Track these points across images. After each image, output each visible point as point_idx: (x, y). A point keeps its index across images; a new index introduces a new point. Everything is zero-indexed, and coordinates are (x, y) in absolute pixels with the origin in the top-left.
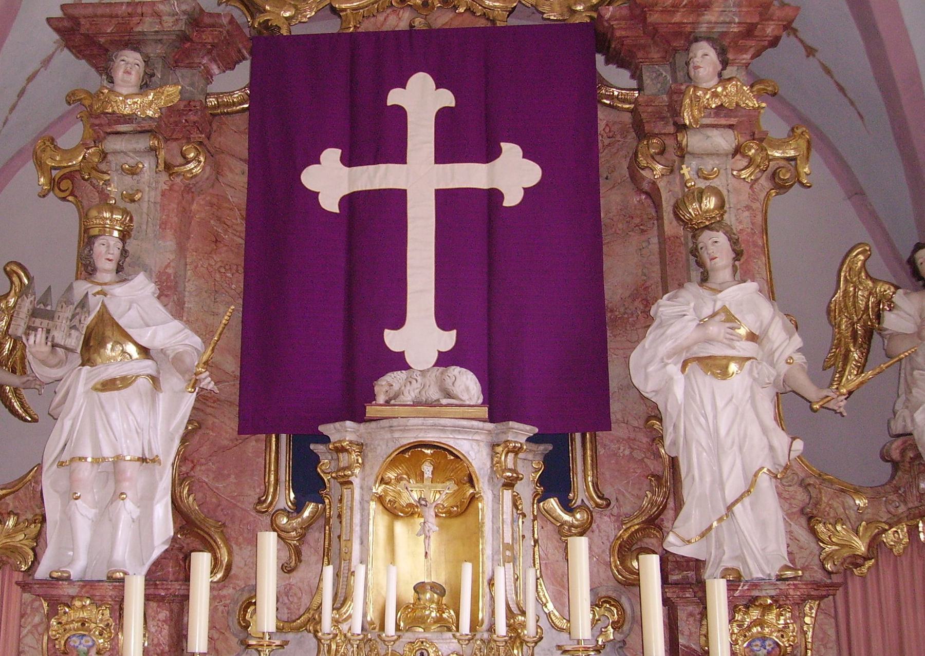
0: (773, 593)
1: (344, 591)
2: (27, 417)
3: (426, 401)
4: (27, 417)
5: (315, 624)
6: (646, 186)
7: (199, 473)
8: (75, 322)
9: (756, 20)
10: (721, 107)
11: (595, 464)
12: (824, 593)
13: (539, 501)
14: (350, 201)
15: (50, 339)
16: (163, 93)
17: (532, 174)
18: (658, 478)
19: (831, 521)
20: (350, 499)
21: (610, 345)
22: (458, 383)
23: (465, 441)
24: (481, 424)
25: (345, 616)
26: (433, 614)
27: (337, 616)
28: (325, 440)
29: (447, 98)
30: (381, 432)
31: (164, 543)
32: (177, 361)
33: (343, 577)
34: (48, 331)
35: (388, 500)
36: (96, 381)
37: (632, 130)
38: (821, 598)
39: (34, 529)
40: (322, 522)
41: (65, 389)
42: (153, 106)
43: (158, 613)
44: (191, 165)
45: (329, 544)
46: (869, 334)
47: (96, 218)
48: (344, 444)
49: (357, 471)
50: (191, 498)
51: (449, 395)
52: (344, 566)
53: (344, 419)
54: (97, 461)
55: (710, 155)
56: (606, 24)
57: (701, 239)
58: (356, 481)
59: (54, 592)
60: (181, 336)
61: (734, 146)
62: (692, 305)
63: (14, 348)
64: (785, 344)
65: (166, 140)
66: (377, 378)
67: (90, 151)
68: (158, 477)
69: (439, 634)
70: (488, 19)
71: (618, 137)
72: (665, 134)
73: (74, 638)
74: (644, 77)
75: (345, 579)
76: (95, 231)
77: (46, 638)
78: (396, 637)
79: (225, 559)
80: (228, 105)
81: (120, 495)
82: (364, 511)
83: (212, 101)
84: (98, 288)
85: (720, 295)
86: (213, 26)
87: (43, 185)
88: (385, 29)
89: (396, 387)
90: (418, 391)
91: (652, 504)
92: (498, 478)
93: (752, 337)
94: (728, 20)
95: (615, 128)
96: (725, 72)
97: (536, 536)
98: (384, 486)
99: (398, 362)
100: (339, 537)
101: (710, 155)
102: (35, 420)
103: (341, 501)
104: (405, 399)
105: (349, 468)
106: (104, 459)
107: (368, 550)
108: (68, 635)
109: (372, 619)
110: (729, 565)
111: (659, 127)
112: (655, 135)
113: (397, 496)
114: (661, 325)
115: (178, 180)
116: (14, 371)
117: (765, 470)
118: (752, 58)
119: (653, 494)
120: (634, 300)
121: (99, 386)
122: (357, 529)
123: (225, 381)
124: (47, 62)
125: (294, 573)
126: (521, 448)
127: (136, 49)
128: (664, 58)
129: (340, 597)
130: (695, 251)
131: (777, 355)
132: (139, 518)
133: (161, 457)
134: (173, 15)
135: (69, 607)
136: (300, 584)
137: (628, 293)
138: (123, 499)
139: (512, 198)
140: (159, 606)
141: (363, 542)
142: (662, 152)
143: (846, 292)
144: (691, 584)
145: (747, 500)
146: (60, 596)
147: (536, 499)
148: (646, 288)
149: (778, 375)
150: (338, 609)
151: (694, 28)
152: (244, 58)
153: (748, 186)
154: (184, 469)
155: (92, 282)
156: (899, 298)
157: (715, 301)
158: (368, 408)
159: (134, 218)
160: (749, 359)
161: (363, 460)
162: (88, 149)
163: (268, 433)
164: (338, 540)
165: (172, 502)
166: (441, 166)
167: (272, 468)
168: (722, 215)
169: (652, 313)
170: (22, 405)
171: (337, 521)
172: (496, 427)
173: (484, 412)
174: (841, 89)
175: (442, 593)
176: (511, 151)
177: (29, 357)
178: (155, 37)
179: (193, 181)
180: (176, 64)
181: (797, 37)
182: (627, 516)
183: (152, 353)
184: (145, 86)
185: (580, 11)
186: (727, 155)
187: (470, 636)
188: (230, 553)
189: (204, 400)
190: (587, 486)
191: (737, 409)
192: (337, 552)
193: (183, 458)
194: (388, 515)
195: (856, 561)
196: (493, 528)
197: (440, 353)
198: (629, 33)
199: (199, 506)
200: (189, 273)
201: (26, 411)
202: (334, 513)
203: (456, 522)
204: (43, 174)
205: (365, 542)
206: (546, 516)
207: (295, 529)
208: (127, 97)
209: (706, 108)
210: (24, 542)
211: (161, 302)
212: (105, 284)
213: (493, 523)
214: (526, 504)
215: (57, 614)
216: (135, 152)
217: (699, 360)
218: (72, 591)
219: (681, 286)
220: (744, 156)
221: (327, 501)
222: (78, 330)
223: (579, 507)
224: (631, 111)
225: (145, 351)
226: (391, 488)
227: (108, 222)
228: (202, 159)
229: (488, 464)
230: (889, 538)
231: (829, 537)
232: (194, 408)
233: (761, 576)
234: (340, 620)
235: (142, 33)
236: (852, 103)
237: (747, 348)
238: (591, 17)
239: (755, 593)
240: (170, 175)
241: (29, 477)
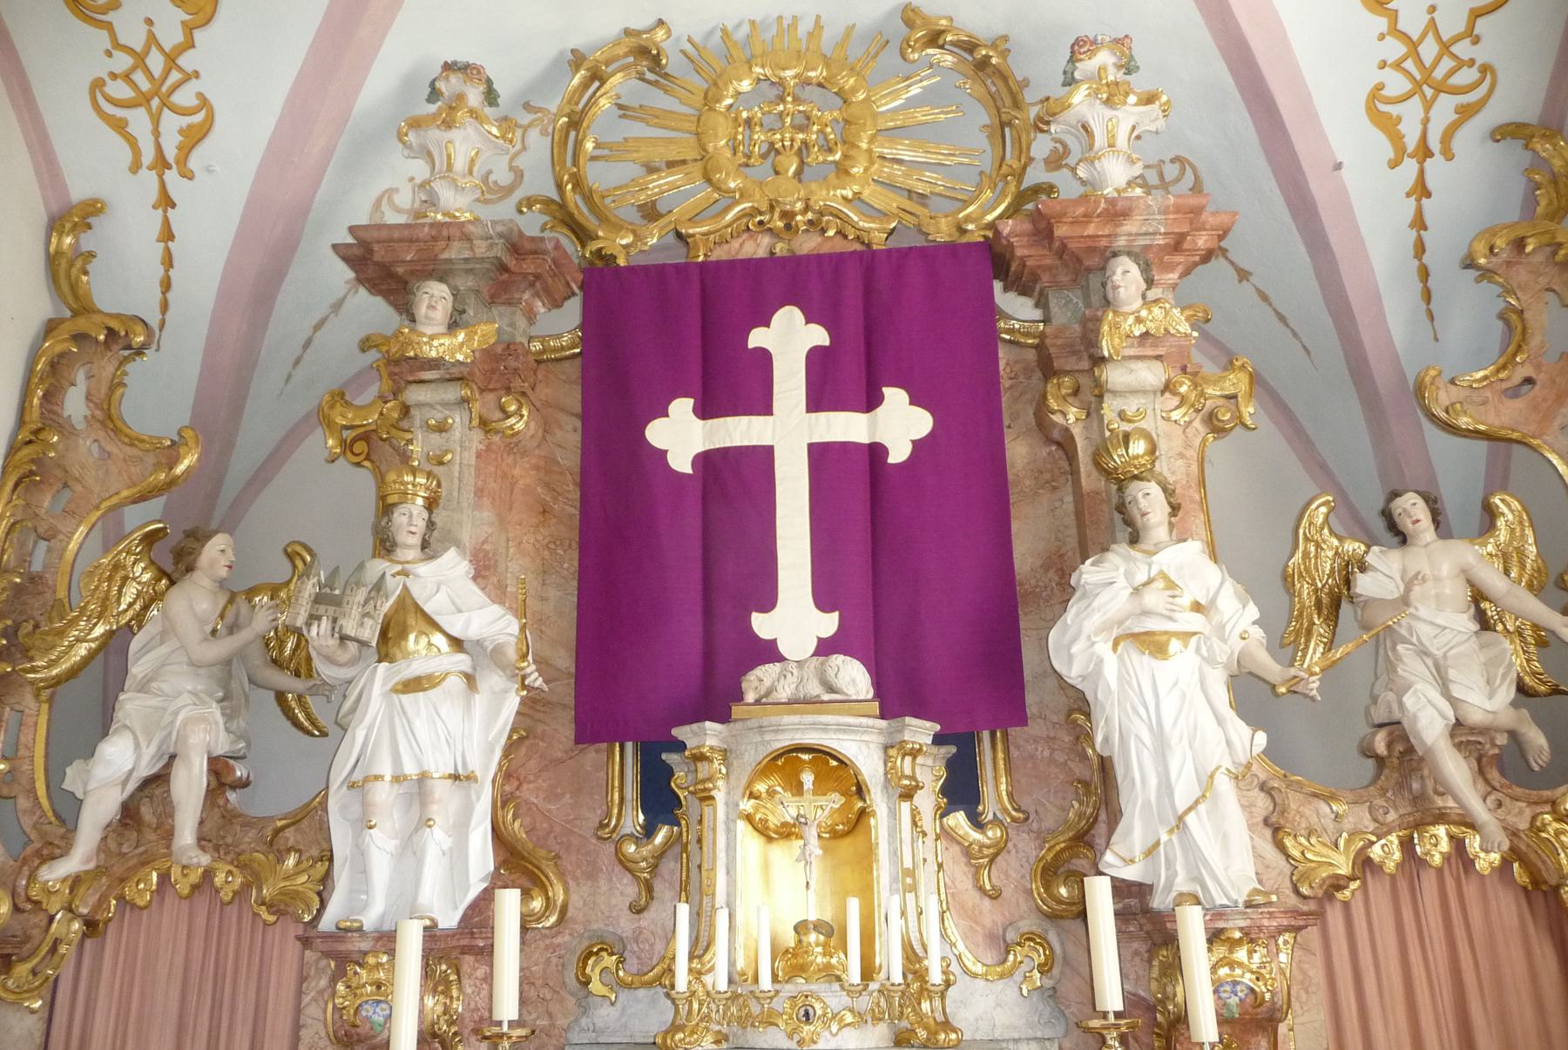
0: (1242, 923)
2: (312, 729)
4: (312, 729)
6: (1056, 435)
7: (527, 793)
8: (369, 608)
9: (1185, 230)
10: (1147, 334)
11: (1009, 771)
12: (1302, 923)
13: (942, 816)
14: (706, 461)
15: (337, 629)
16: (476, 333)
17: (921, 423)
18: (1086, 784)
19: (1303, 832)
21: (1022, 625)
24: (870, 722)
28: (680, 746)
29: (819, 336)
31: (482, 880)
32: (495, 656)
34: (335, 620)
36: (396, 680)
37: (1037, 369)
38: (1297, 930)
39: (321, 868)
40: (677, 849)
41: (356, 693)
42: (464, 349)
43: (475, 969)
44: (512, 421)
45: (688, 876)
46: (1336, 604)
47: (395, 482)
49: (720, 783)
50: (517, 824)
51: (831, 689)
54: (398, 779)
55: (1134, 392)
56: (1004, 242)
57: (1128, 491)
58: (720, 796)
59: (342, 947)
60: (501, 624)
61: (1163, 380)
62: (1122, 570)
63: (298, 645)
64: (1238, 615)
65: (482, 391)
66: (745, 673)
67: (388, 405)
68: (474, 797)
69: (827, 985)
70: (863, 243)
71: (1021, 378)
72: (1078, 371)
73: (366, 1006)
74: (1051, 305)
76: (391, 500)
77: (330, 1006)
79: (560, 898)
80: (555, 350)
81: (427, 822)
83: (537, 346)
84: (398, 568)
85: (1155, 558)
86: (535, 252)
87: (332, 447)
88: (740, 257)
89: (767, 683)
90: (793, 686)
91: (1080, 817)
93: (1197, 607)
94: (1151, 230)
95: (1018, 367)
96: (1148, 293)
99: (769, 652)
100: (700, 867)
101: (1134, 392)
102: (324, 734)
103: (700, 822)
105: (709, 779)
106: (405, 778)
107: (735, 881)
108: (359, 1002)
110: (1185, 889)
111: (1070, 363)
112: (1067, 373)
114: (1084, 595)
115: (496, 438)
116: (297, 674)
117: (1223, 770)
118: (1180, 278)
119: (1081, 803)
120: (1047, 571)
121: (400, 687)
123: (557, 680)
124: (337, 306)
125: (645, 914)
126: (920, 750)
127: (441, 280)
128: (1074, 280)
130: (1122, 508)
131: (1228, 629)
132: (451, 849)
133: (478, 774)
134: (487, 239)
135: (360, 965)
136: (652, 927)
137: (1039, 563)
138: (430, 826)
139: (899, 453)
140: (477, 960)
141: (730, 871)
142: (1076, 392)
143: (1306, 554)
144: (1135, 914)
145: (1202, 807)
146: (351, 952)
148: (1062, 556)
149: (1232, 653)
151: (1110, 242)
152: (574, 294)
153: (1181, 430)
154: (507, 788)
155: (391, 561)
156: (1374, 557)
157: (1150, 565)
158: (734, 708)
159: (444, 484)
160: (1195, 634)
162: (386, 402)
163: (611, 741)
165: (493, 829)
166: (813, 415)
167: (616, 784)
168: (1154, 462)
169: (1073, 582)
170: (309, 716)
171: (697, 846)
173: (875, 707)
174: (1282, 318)
175: (829, 935)
176: (895, 397)
177: (313, 654)
178: (463, 267)
179: (515, 440)
180: (493, 300)
181: (1227, 258)
182: (1049, 831)
183: (466, 645)
184: (453, 326)
185: (972, 231)
186: (1155, 393)
188: (566, 891)
189: (532, 705)
190: (999, 796)
191: (1184, 695)
192: (698, 885)
193: (508, 774)
195: (1337, 884)
197: (820, 640)
198: (1032, 252)
199: (526, 832)
200: (512, 550)
201: (313, 724)
202: (692, 837)
203: (846, 843)
204: (332, 434)
205: (732, 873)
206: (946, 834)
207: (645, 859)
208: (432, 338)
209: (1128, 336)
210: (308, 885)
211: (477, 584)
212: (408, 562)
214: (928, 821)
215: (345, 974)
216: (445, 404)
217: (1134, 636)
218: (365, 945)
219: (1105, 549)
220: (1175, 393)
221: (683, 822)
222: (372, 618)
223: (990, 822)
224: (1036, 347)
225: (457, 644)
227: (410, 487)
228: (525, 412)
229: (881, 770)
230: (1376, 852)
231: (1303, 853)
232: (518, 713)
233: (1225, 902)
235: (449, 261)
236: (1295, 334)
237: (1193, 622)
238: (984, 236)
239: (1220, 924)
240: (487, 432)
241: (315, 803)
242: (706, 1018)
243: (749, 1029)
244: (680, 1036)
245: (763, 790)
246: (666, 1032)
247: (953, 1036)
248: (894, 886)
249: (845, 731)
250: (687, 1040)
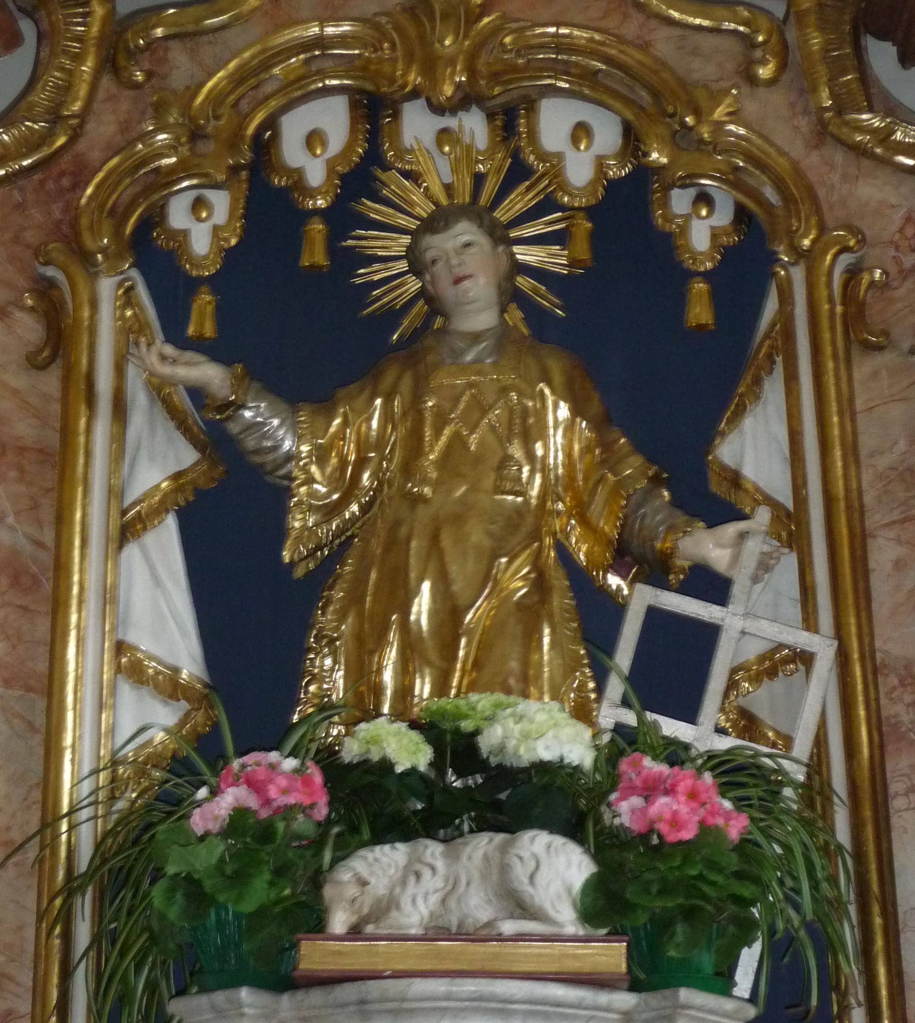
3: (459, 926)
22: (542, 877)
89: (379, 886)
104: (403, 920)
158: (306, 947)
172: (646, 1002)
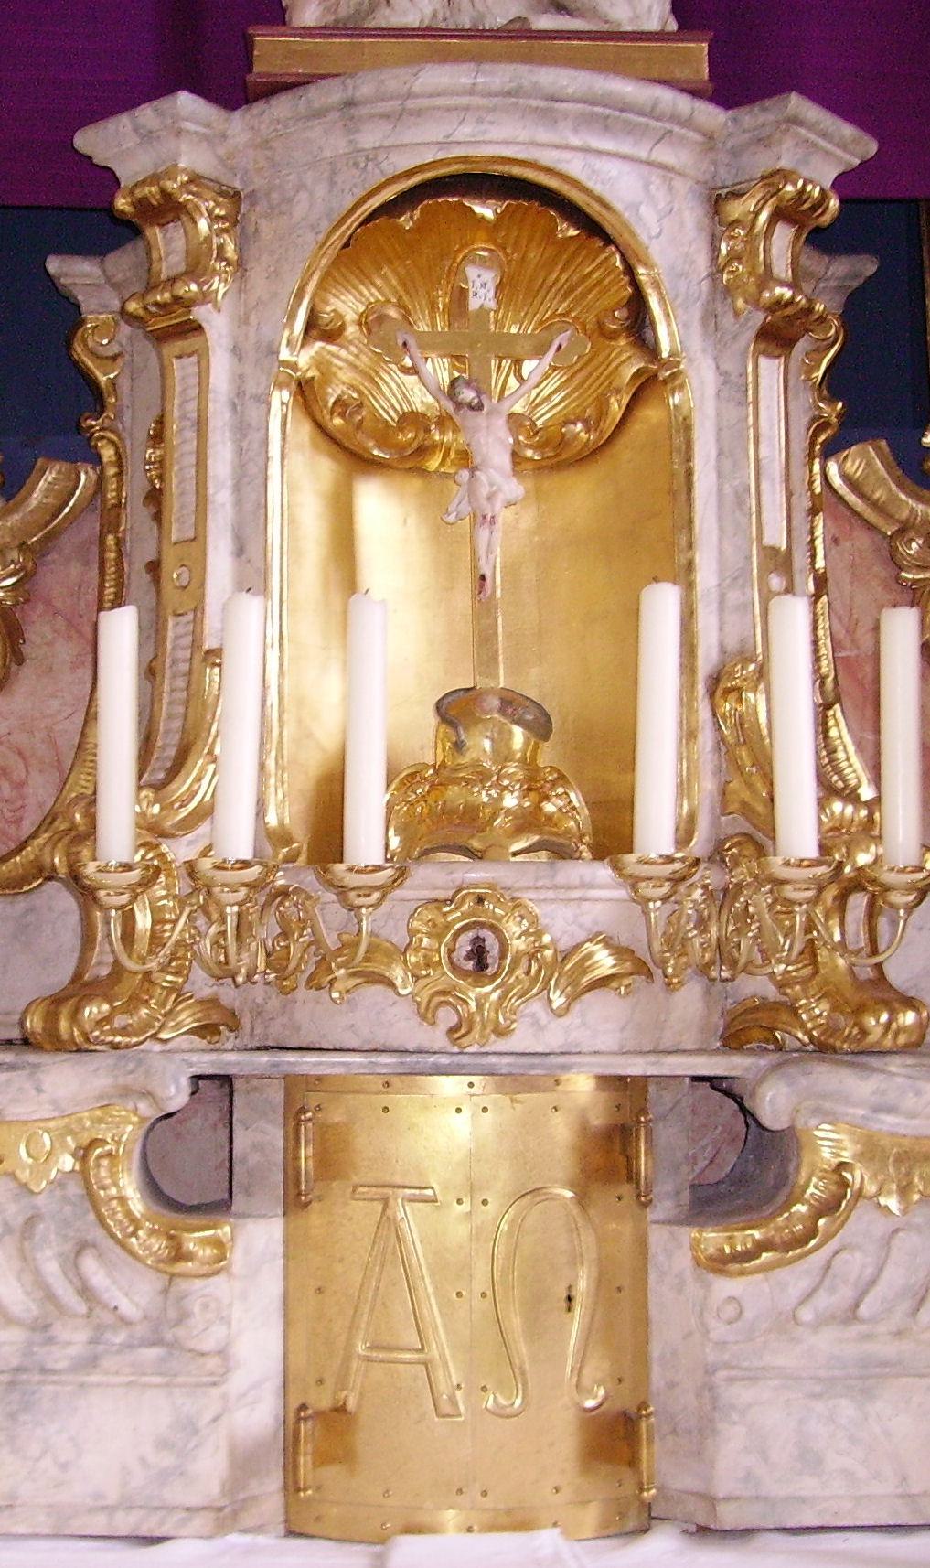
1: (177, 724)
5: (72, 842)
20: (194, 392)
23: (626, 167)
24: (684, 104)
25: (184, 813)
26: (510, 801)
27: (156, 809)
30: (310, 134)
33: (174, 677)
35: (332, 400)
48: (172, 186)
52: (177, 638)
53: (162, 88)
58: (217, 324)
75: (181, 683)
78: (389, 872)
82: (248, 433)
92: (737, 314)
97: (820, 563)
98: (319, 345)
103: (158, 437)
109: (281, 822)
113: (365, 386)
122: (221, 496)
129: (163, 748)
136: (20, 739)
147: (822, 438)
150: (159, 787)
161: (240, 250)
164: (147, 577)
187: (677, 866)
194: (333, 457)
196: (720, 490)
202: (135, 488)
205: (253, 550)
213: (720, 475)
221: (108, 453)
226: (343, 353)
229: (702, 263)
234: (168, 824)
242: (181, 957)
243: (302, 993)
244: (93, 1011)
245: (350, 316)
246: (57, 1001)
247: (909, 1018)
248: (733, 597)
249: (606, 126)
250: (120, 1021)
